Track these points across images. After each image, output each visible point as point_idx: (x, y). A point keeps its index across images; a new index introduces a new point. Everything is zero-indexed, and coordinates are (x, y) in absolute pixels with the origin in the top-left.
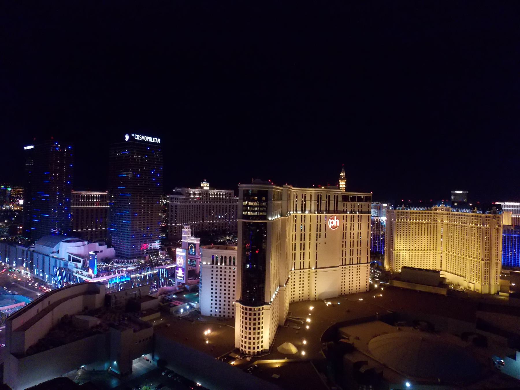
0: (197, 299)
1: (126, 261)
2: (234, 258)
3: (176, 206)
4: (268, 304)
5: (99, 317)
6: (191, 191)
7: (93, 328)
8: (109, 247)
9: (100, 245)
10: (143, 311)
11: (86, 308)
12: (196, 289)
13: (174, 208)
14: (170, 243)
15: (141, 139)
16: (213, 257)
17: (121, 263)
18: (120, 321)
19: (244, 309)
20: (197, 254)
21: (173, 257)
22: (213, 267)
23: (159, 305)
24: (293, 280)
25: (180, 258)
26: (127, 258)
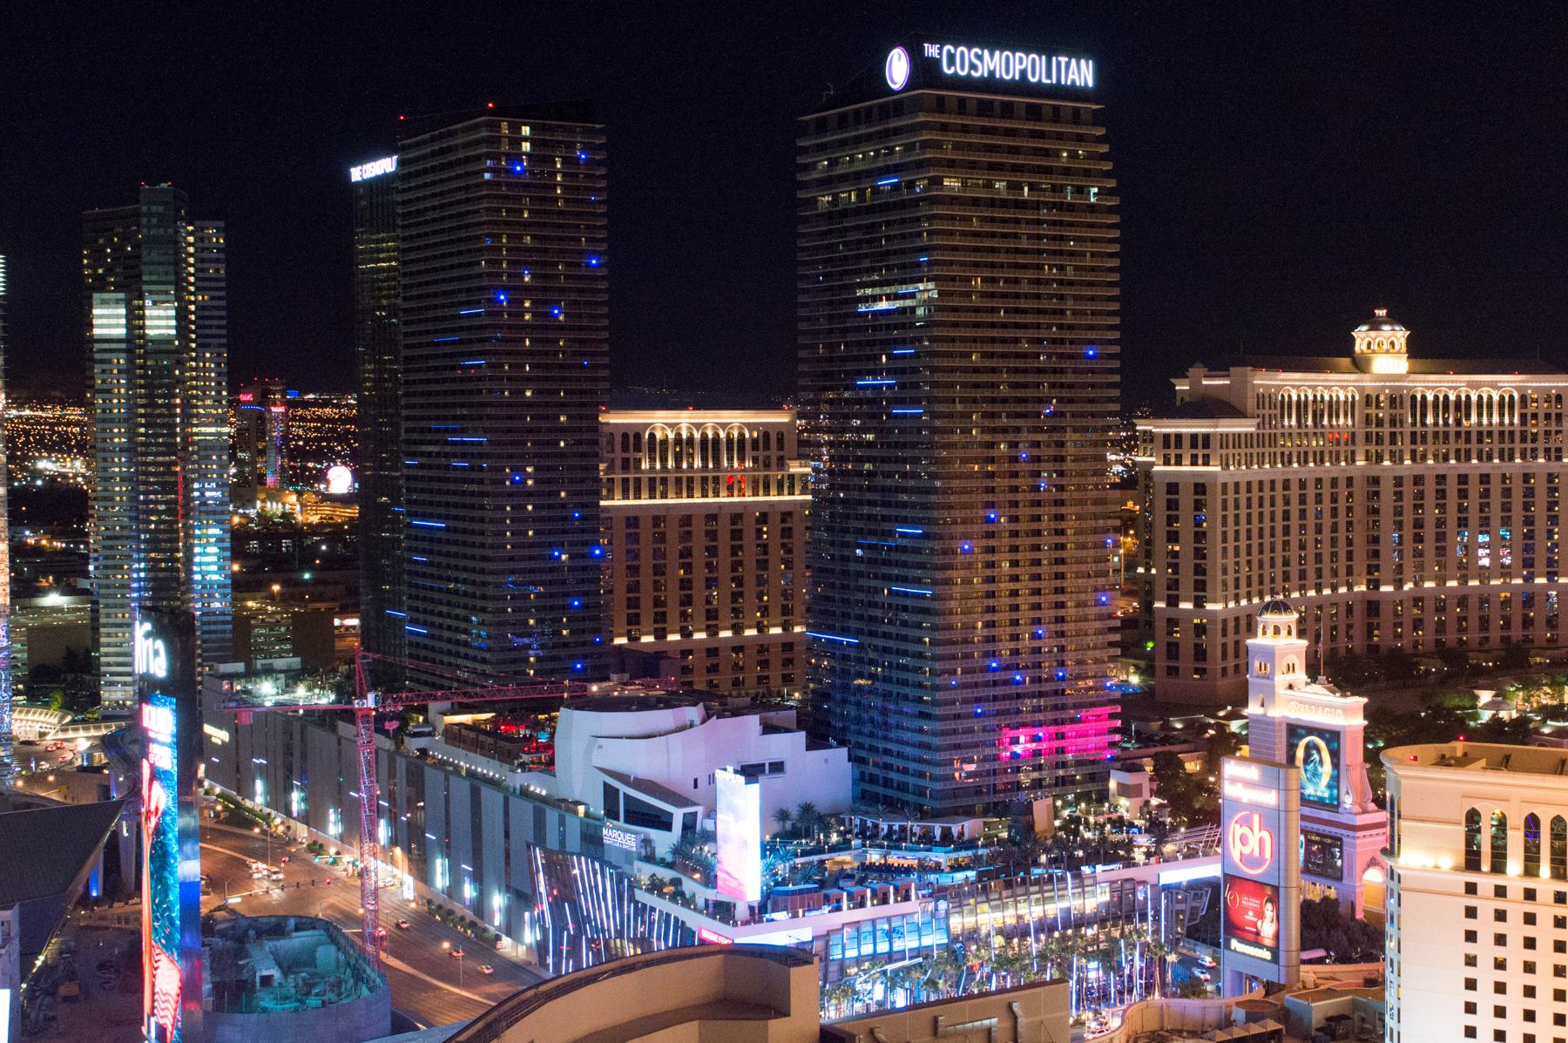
1: (916, 827)
3: (1200, 488)
6: (1293, 384)
9: (768, 728)
13: (1186, 499)
15: (981, 72)
16: (1473, 817)
17: (896, 840)
21: (1196, 809)
22: (1471, 889)
25: (1246, 822)
26: (923, 814)
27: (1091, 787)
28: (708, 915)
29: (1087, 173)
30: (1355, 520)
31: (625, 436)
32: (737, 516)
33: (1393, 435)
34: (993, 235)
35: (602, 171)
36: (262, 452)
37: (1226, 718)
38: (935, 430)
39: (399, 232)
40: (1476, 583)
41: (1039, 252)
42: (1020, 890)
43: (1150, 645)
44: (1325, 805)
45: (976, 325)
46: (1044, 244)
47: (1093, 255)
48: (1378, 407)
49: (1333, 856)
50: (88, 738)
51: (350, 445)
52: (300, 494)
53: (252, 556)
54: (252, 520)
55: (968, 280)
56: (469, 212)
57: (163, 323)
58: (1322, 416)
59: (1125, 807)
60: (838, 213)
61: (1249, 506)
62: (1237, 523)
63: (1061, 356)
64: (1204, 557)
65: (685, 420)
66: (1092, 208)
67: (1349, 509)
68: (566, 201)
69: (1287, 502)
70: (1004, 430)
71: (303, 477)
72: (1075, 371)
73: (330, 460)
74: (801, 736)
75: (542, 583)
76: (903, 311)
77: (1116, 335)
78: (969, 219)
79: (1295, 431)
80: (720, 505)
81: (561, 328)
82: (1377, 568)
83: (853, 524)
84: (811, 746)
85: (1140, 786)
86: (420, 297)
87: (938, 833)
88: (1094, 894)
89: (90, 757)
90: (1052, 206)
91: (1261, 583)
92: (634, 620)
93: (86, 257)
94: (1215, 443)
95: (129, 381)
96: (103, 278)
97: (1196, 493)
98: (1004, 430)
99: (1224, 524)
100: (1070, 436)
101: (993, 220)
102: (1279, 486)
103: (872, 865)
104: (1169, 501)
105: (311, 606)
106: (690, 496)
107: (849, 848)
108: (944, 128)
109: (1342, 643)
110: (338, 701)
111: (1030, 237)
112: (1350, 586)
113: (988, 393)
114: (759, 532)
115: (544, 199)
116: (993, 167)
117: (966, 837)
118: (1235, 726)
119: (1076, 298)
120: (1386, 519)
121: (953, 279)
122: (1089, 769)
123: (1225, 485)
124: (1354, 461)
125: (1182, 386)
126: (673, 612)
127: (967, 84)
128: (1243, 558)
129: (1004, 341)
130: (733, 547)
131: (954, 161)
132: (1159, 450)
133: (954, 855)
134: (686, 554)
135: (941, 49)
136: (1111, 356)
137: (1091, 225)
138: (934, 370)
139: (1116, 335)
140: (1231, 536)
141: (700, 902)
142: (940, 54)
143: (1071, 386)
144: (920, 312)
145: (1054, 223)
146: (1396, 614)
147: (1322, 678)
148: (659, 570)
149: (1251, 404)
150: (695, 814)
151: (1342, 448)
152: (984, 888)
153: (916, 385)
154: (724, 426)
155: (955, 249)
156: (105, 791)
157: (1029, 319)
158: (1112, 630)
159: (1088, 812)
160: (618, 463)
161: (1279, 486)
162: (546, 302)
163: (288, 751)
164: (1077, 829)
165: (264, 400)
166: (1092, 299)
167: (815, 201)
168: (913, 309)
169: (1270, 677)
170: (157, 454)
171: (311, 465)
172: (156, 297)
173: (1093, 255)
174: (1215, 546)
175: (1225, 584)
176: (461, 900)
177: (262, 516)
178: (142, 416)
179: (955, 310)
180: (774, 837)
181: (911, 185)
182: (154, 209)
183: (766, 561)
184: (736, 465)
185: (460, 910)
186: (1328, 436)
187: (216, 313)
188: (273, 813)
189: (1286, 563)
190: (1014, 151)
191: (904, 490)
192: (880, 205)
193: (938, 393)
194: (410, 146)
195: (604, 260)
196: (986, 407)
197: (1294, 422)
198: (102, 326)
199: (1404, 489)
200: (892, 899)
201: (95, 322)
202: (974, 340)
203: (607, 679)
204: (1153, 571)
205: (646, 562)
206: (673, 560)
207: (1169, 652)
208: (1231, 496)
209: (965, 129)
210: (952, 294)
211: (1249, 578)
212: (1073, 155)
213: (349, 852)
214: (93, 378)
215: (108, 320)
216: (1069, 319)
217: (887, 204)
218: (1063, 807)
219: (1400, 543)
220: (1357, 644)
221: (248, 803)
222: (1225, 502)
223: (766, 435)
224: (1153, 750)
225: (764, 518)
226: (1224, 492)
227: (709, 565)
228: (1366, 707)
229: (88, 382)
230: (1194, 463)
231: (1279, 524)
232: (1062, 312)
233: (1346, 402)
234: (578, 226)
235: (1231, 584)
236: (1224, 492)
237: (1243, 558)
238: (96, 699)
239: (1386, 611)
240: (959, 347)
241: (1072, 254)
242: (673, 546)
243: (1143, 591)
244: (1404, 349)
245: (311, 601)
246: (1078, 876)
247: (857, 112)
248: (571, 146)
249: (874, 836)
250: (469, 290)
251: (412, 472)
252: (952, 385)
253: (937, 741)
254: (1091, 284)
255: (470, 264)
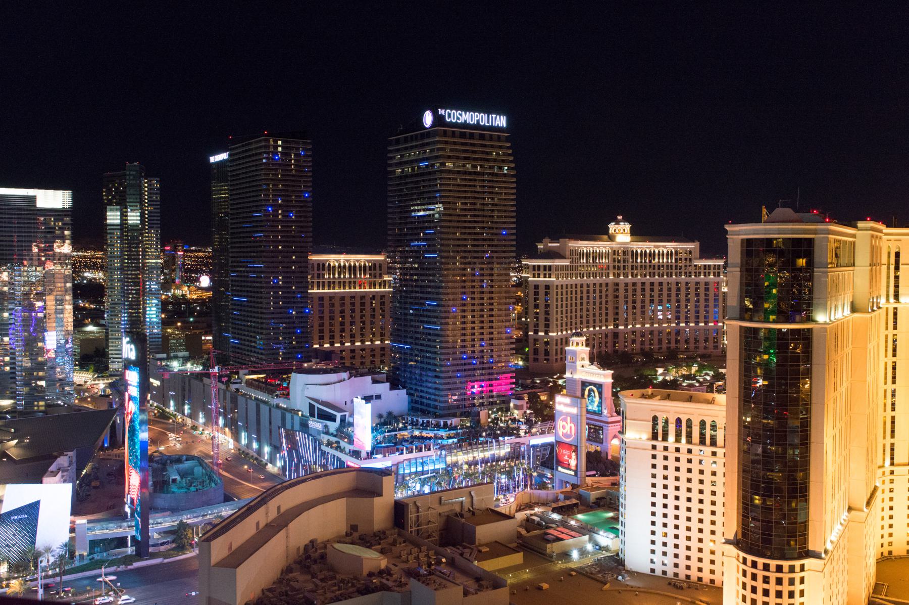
0: (613, 525)
2: (714, 427)
3: (547, 287)
4: (817, 556)
5: (382, 552)
6: (584, 246)
7: (371, 575)
8: (393, 387)
9: (375, 381)
10: (480, 545)
11: (354, 528)
12: (610, 502)
14: (533, 382)
15: (461, 121)
18: (430, 565)
19: (749, 563)
20: (605, 412)
21: (544, 415)
22: (654, 447)
23: (520, 536)
24: (888, 495)
25: (565, 420)
26: (436, 416)
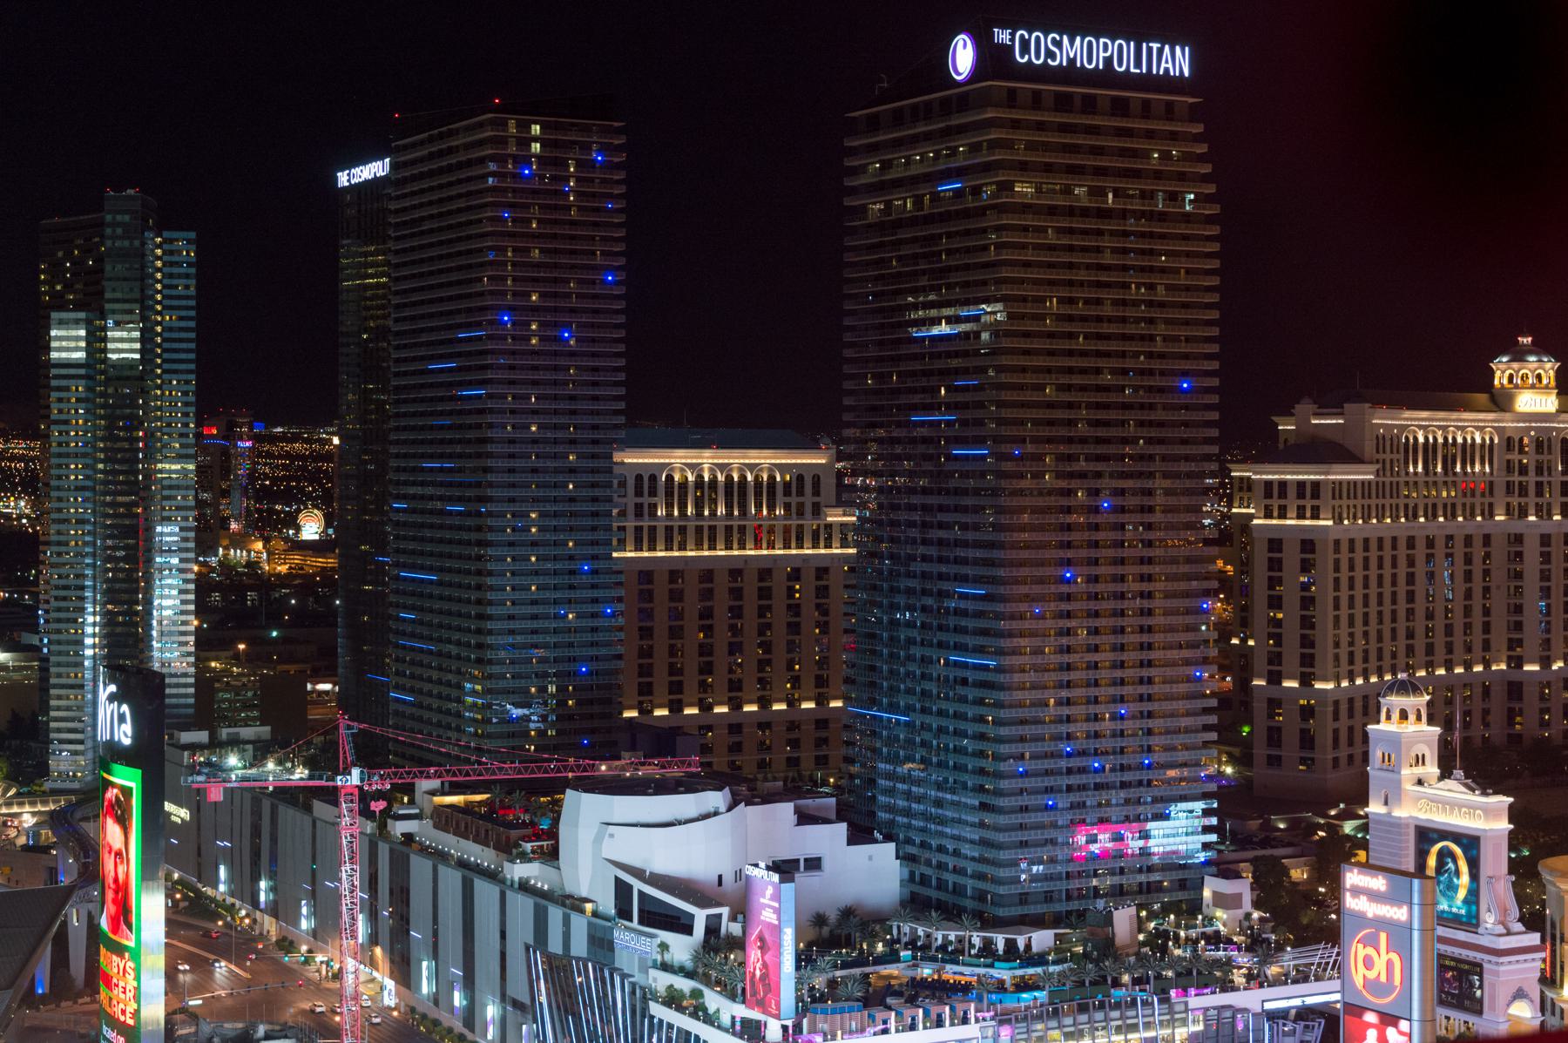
6: (1420, 425)
9: (804, 818)
25: (1372, 942)
27: (1181, 895)
28: (734, 1034)
29: (1182, 177)
30: (1493, 585)
31: (639, 478)
32: (765, 571)
33: (1539, 485)
34: (1071, 248)
35: (621, 176)
36: (225, 493)
37: (1338, 817)
38: (1000, 475)
39: (391, 245)
40: (781, 706)
41: (1125, 268)
42: (1099, 1016)
43: (1246, 729)
44: (1461, 923)
45: (1051, 353)
46: (1131, 260)
47: (1188, 271)
48: (1521, 451)
49: (1472, 985)
50: (34, 814)
51: (321, 485)
52: (266, 540)
53: (214, 610)
54: (213, 570)
55: (1042, 300)
56: (470, 223)
57: (126, 346)
58: (1454, 463)
59: (1223, 919)
60: (892, 224)
61: (1366, 567)
62: (1366, 586)
63: (1150, 389)
64: (1312, 627)
65: (707, 459)
66: (1187, 218)
67: (1486, 573)
68: (580, 209)
69: (1411, 562)
70: (1082, 475)
71: (272, 522)
72: (1165, 407)
73: (298, 502)
74: (842, 828)
75: (546, 646)
76: (965, 336)
77: (1215, 365)
78: (1044, 230)
79: (1421, 480)
80: (747, 558)
81: (572, 354)
82: (1520, 643)
83: (905, 583)
84: (853, 840)
85: (1240, 896)
86: (413, 318)
87: (1001, 946)
88: (1184, 1022)
89: (37, 835)
90: (1142, 214)
91: (1380, 658)
92: (646, 690)
93: (43, 272)
94: (1326, 493)
95: (87, 411)
96: (61, 295)
97: (1303, 551)
98: (1082, 475)
99: (1337, 588)
100: (1159, 483)
101: (1071, 231)
102: (1402, 544)
103: (924, 980)
104: (1270, 560)
105: (280, 668)
106: (712, 547)
107: (898, 960)
108: (1015, 124)
109: (1478, 731)
110: (311, 777)
111: (1114, 251)
112: (1487, 665)
113: (1063, 432)
114: (791, 591)
115: (556, 208)
116: (1073, 170)
117: (1035, 949)
118: (1348, 827)
119: (1168, 322)
120: (1531, 583)
121: (1024, 299)
122: (1180, 875)
123: (1337, 542)
124: (1492, 515)
125: (1286, 426)
126: (691, 680)
127: (1031, 72)
128: (1359, 628)
129: (1083, 371)
130: (760, 607)
131: (1026, 163)
132: (1276, 501)
133: (1020, 972)
134: (706, 614)
135: (1013, 35)
136: (1208, 390)
137: (1185, 238)
138: (1001, 404)
139: (1215, 365)
140: (1344, 603)
141: (726, 1020)
142: (1012, 40)
143: (1161, 424)
144: (985, 336)
145: (1143, 235)
146: (1542, 697)
147: (1459, 773)
148: (675, 632)
149: (1369, 449)
150: (720, 916)
151: (1478, 500)
152: (1056, 1012)
153: (980, 423)
154: (751, 467)
155: (1027, 264)
156: (53, 873)
157: (1114, 346)
158: (1207, 711)
159: (1178, 926)
160: (631, 510)
161: (1402, 544)
162: (556, 325)
163: (256, 832)
164: (1165, 945)
165: (230, 434)
166: (1187, 323)
167: (864, 208)
168: (977, 334)
169: (1395, 770)
170: (115, 493)
171: (278, 507)
172: (119, 317)
173: (1188, 271)
174: (1324, 613)
175: (1337, 658)
176: (451, 1009)
177: (225, 565)
178: (101, 450)
179: (1027, 335)
180: (809, 945)
181: (976, 191)
182: (119, 218)
183: (798, 625)
184: (765, 512)
185: (447, 1020)
186: (1460, 486)
187: (183, 335)
188: (238, 903)
189: (1410, 635)
190: (1097, 151)
191: (965, 544)
192: (940, 214)
193: (1006, 431)
194: (405, 147)
195: (622, 276)
196: (1063, 449)
197: (1420, 469)
198: (59, 349)
199: (1553, 549)
200: (921, 1026)
201: (54, 344)
202: (1049, 370)
203: (619, 758)
204: (1251, 643)
205: (661, 623)
206: (691, 621)
207: (1302, 740)
208: (1344, 557)
209: (1040, 126)
210: (1023, 317)
211: (1366, 652)
212: (1165, 156)
213: (323, 951)
214: (48, 407)
215: (67, 344)
216: (1159, 346)
217: (949, 212)
218: (1149, 919)
219: (1548, 614)
220: (1496, 732)
221: (209, 891)
222: (1337, 562)
223: (800, 478)
224: (1251, 854)
225: (796, 575)
226: (1337, 550)
227: (733, 628)
228: (1511, 807)
229: (42, 412)
230: (1301, 516)
231: (1402, 589)
232: (1152, 338)
233: (1483, 445)
234: (593, 238)
235: (1344, 658)
236: (1337, 550)
237: (1359, 628)
238: (43, 770)
239: (1530, 694)
240: (1029, 379)
241: (1163, 270)
242: (692, 605)
243: (1238, 663)
244: (1553, 383)
245: (279, 662)
246: (1165, 1000)
247: (915, 107)
248: (586, 147)
249: (926, 947)
250: (469, 310)
251: (402, 517)
252: (1022, 422)
253: (1002, 838)
254: (1185, 306)
255: (470, 281)
